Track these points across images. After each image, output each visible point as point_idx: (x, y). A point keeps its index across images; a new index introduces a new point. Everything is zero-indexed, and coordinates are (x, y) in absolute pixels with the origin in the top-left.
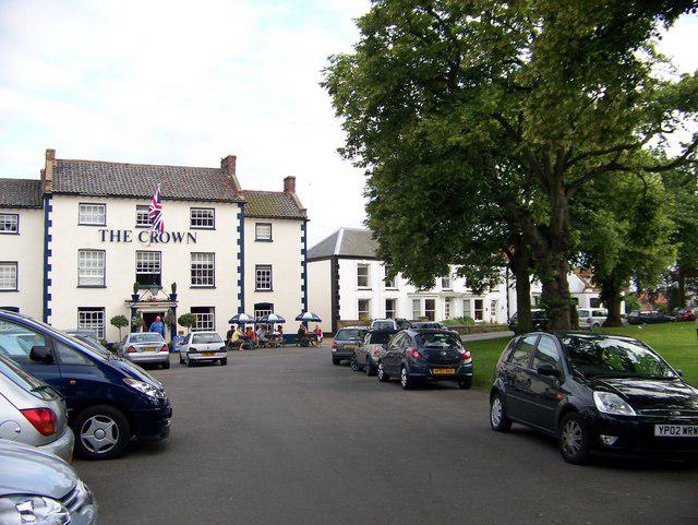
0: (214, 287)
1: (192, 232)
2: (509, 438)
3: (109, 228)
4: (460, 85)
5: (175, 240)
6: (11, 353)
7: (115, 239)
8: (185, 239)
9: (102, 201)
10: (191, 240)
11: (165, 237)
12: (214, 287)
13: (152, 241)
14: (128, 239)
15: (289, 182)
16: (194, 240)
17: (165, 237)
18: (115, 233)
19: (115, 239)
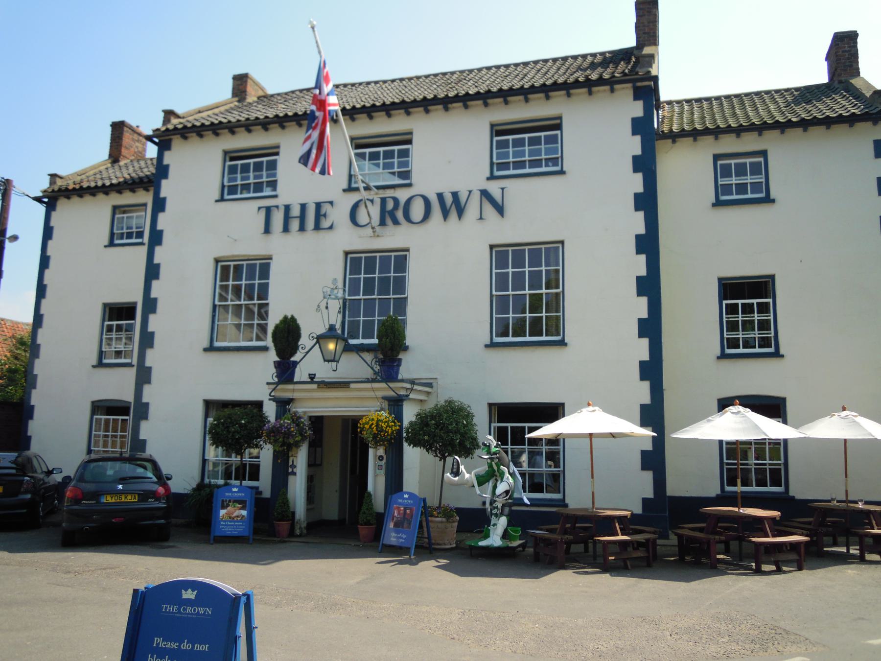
0: (562, 343)
1: (494, 188)
2: (313, 373)
3: (281, 201)
4: (279, 461)
5: (446, 214)
6: (32, 197)
7: (295, 225)
8: (472, 210)
9: (397, 124)
10: (489, 209)
11: (417, 209)
12: (562, 343)
13: (383, 223)
14: (325, 224)
15: (49, 175)
16: (500, 209)
17: (417, 209)
18: (296, 211)
19: (295, 225)
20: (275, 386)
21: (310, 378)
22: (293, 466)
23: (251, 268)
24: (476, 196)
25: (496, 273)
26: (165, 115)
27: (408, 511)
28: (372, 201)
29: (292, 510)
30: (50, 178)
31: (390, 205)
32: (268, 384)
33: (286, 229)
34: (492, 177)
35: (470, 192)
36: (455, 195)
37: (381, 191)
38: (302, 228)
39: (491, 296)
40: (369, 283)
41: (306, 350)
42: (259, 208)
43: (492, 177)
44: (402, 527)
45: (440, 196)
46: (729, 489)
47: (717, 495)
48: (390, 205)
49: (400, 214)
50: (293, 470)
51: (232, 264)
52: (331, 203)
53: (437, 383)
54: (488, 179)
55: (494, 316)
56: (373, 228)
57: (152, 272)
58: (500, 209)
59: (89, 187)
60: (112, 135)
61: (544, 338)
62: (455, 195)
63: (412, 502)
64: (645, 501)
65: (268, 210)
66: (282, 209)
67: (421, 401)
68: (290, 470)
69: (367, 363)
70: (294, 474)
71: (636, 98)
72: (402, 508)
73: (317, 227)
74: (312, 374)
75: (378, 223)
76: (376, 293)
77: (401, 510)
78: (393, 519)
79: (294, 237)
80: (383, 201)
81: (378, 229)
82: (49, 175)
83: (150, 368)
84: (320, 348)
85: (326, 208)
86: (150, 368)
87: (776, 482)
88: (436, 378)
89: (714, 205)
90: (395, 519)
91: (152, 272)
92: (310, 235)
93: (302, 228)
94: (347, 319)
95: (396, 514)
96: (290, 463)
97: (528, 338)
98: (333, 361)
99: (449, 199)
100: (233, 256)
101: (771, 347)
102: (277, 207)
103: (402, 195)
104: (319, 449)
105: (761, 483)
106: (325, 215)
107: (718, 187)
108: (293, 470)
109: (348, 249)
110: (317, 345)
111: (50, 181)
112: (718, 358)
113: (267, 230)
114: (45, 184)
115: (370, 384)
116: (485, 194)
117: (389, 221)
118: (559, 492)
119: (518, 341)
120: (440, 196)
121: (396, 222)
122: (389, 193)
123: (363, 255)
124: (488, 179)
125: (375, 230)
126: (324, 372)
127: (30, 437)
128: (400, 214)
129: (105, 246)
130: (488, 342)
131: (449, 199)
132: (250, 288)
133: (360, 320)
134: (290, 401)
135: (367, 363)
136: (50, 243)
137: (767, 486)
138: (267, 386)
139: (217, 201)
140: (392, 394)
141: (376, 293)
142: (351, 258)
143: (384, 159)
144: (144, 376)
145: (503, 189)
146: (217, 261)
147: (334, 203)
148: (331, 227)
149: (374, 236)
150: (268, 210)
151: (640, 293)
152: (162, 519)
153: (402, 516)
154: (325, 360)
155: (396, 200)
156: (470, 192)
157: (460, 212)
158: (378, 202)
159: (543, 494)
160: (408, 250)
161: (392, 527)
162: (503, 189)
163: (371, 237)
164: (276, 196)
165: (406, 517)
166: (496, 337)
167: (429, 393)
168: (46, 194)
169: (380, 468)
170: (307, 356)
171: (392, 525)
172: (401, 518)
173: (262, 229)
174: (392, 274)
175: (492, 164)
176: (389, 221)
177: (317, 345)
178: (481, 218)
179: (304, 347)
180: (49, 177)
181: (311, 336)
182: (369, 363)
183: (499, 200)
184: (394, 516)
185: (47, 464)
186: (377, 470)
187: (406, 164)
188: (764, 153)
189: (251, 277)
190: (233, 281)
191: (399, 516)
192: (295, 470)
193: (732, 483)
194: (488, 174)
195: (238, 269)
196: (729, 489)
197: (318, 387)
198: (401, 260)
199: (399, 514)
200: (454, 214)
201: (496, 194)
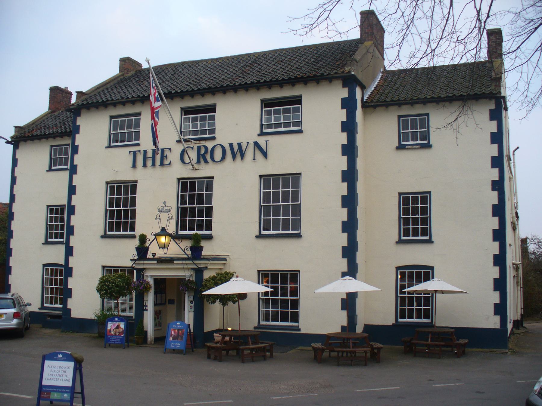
1: (262, 141)
3: (141, 148)
5: (234, 157)
9: (207, 101)
10: (259, 154)
13: (198, 162)
14: (166, 162)
16: (265, 154)
19: (149, 163)
20: (134, 261)
21: (153, 255)
22: (146, 306)
23: (126, 187)
24: (251, 145)
25: (263, 192)
26: (77, 94)
27: (180, 331)
28: (192, 148)
29: (145, 330)
30: (15, 129)
31: (203, 151)
32: (131, 260)
33: (145, 165)
34: (262, 134)
35: (248, 143)
36: (239, 145)
37: (198, 142)
38: (154, 165)
39: (261, 206)
40: (192, 197)
41: (150, 242)
42: (130, 152)
43: (262, 134)
44: (178, 340)
45: (231, 145)
46: (400, 320)
47: (393, 324)
48: (203, 151)
49: (208, 157)
50: (146, 308)
51: (116, 185)
52: (170, 149)
53: (229, 258)
54: (259, 135)
55: (262, 218)
56: (193, 165)
57: (72, 190)
58: (265, 154)
59: (37, 135)
60: (50, 95)
61: (290, 232)
62: (239, 145)
63: (182, 326)
64: (343, 328)
65: (135, 153)
66: (142, 152)
67: (220, 268)
68: (145, 308)
69: (182, 250)
70: (147, 310)
71: (344, 86)
72: (177, 330)
73: (162, 164)
74: (154, 253)
75: (196, 162)
76: (196, 204)
77: (176, 331)
78: (171, 336)
79: (150, 170)
80: (199, 148)
81: (196, 166)
82: (14, 127)
83: (72, 247)
84: (157, 241)
85: (167, 152)
86: (72, 247)
87: (426, 317)
88: (228, 255)
89: (397, 148)
90: (172, 336)
91: (72, 190)
92: (158, 170)
93: (154, 165)
94: (180, 219)
95: (173, 333)
96: (145, 304)
97: (281, 232)
98: (164, 248)
99: (236, 148)
100: (116, 181)
101: (428, 236)
102: (140, 151)
103: (210, 145)
104: (163, 295)
105: (419, 317)
106: (166, 157)
107: (400, 134)
108: (146, 308)
109: (179, 177)
110: (155, 239)
111: (15, 130)
112: (397, 243)
113: (134, 166)
114: (12, 133)
115: (182, 261)
116: (256, 144)
117: (202, 161)
118: (429, 319)
119: (274, 233)
120: (231, 145)
121: (206, 161)
122: (203, 143)
123: (188, 181)
124: (259, 135)
125: (193, 166)
126: (161, 253)
127: (10, 285)
128: (208, 157)
129: (47, 171)
130: (258, 234)
131: (236, 148)
132: (126, 199)
133: (187, 220)
134: (143, 270)
135: (182, 250)
136: (16, 169)
137: (422, 319)
138: (131, 261)
139: (106, 147)
140: (195, 267)
141: (196, 204)
142: (182, 182)
143: (200, 122)
144: (69, 251)
145: (266, 141)
146: (107, 183)
147: (171, 149)
148: (170, 164)
149: (194, 169)
150: (135, 153)
151: (343, 206)
152: (318, 342)
153: (177, 334)
154: (160, 248)
155: (206, 148)
156: (248, 143)
157: (242, 156)
158: (196, 148)
159: (288, 323)
160: (213, 178)
161: (171, 340)
162: (266, 141)
163: (192, 170)
164: (138, 145)
165: (179, 334)
166: (263, 230)
167: (224, 264)
168: (13, 140)
169: (191, 307)
170: (151, 245)
171: (171, 339)
172: (176, 335)
173: (131, 164)
174: (205, 192)
175: (262, 125)
176: (202, 161)
177: (155, 239)
178: (254, 159)
179: (149, 239)
180: (14, 128)
181: (153, 234)
182: (184, 250)
183: (264, 148)
184: (171, 334)
185: (540, 53)
186: (190, 309)
187: (213, 125)
188: (427, 115)
189: (126, 193)
190: (116, 196)
191: (175, 334)
192: (147, 308)
193: (403, 316)
194: (259, 132)
195: (119, 188)
196: (400, 320)
197: (157, 262)
198: (209, 182)
199: (175, 333)
200: (238, 156)
201: (263, 145)
